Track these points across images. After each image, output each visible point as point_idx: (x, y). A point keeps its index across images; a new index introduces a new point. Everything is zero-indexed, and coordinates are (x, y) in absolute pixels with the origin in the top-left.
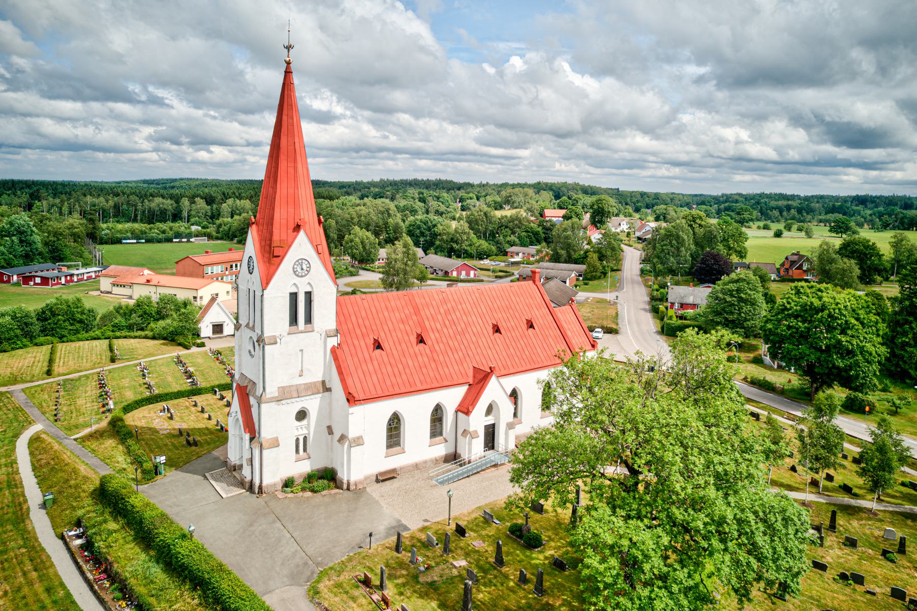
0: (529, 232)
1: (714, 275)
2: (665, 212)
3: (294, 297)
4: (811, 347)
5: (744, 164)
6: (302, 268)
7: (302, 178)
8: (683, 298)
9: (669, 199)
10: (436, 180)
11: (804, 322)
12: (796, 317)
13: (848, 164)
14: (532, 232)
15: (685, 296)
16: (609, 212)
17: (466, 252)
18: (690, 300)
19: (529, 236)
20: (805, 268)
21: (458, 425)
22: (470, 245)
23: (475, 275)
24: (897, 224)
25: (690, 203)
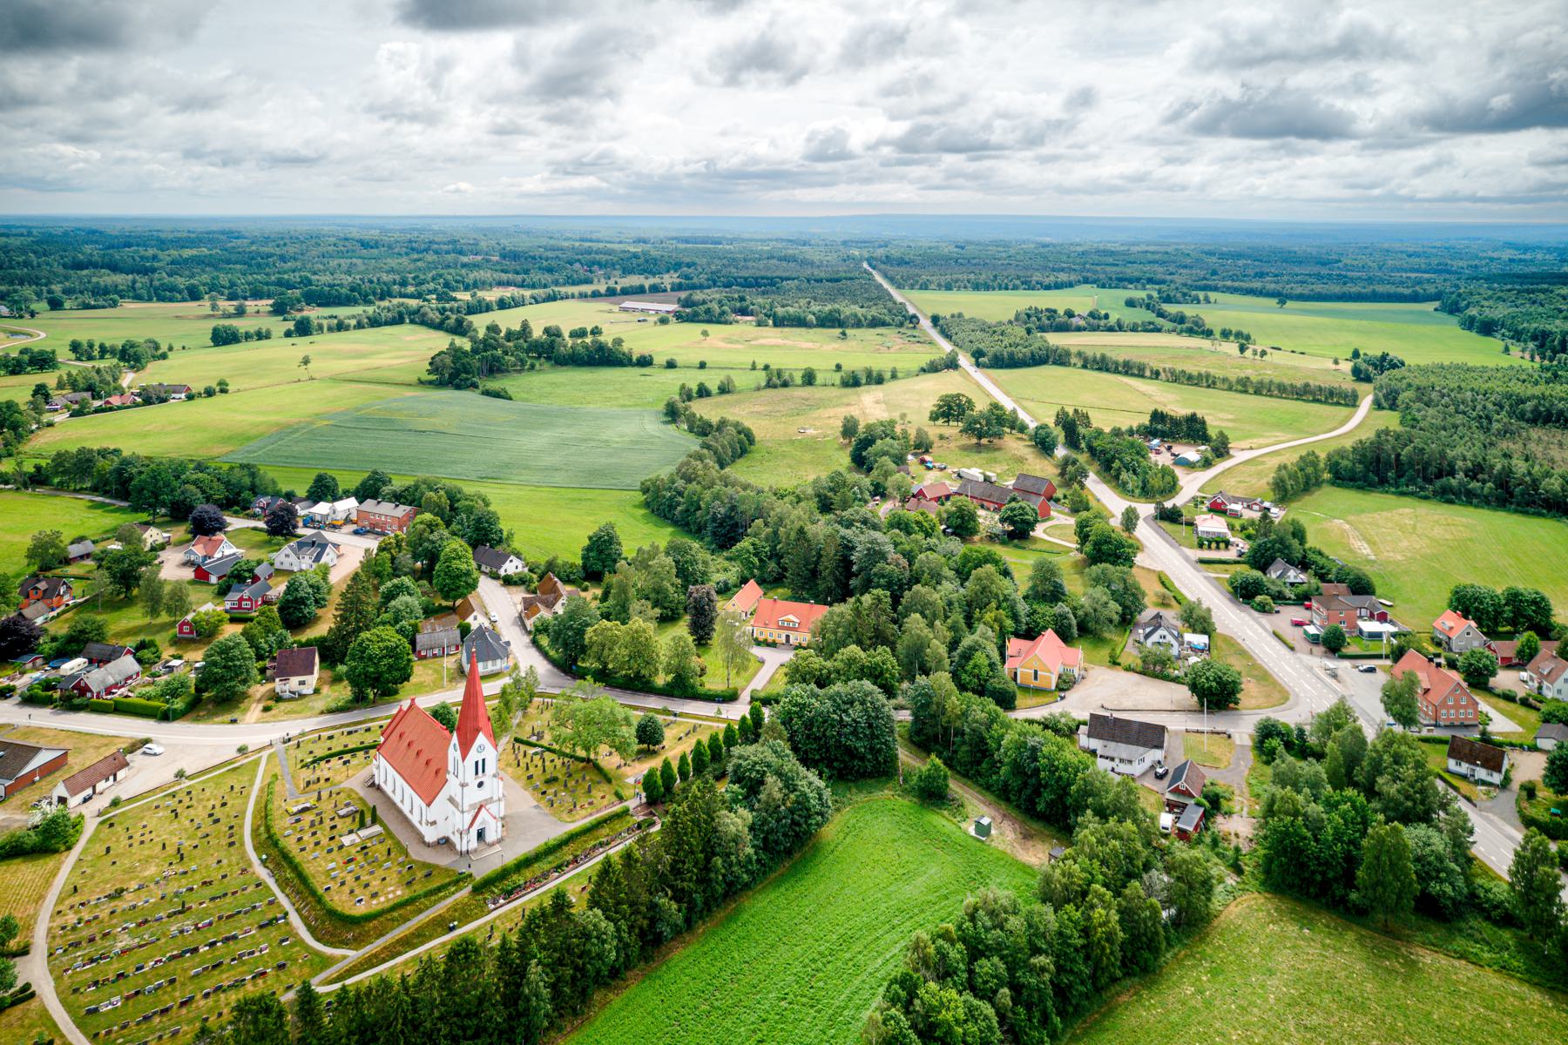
6: (481, 748)
18: (111, 681)
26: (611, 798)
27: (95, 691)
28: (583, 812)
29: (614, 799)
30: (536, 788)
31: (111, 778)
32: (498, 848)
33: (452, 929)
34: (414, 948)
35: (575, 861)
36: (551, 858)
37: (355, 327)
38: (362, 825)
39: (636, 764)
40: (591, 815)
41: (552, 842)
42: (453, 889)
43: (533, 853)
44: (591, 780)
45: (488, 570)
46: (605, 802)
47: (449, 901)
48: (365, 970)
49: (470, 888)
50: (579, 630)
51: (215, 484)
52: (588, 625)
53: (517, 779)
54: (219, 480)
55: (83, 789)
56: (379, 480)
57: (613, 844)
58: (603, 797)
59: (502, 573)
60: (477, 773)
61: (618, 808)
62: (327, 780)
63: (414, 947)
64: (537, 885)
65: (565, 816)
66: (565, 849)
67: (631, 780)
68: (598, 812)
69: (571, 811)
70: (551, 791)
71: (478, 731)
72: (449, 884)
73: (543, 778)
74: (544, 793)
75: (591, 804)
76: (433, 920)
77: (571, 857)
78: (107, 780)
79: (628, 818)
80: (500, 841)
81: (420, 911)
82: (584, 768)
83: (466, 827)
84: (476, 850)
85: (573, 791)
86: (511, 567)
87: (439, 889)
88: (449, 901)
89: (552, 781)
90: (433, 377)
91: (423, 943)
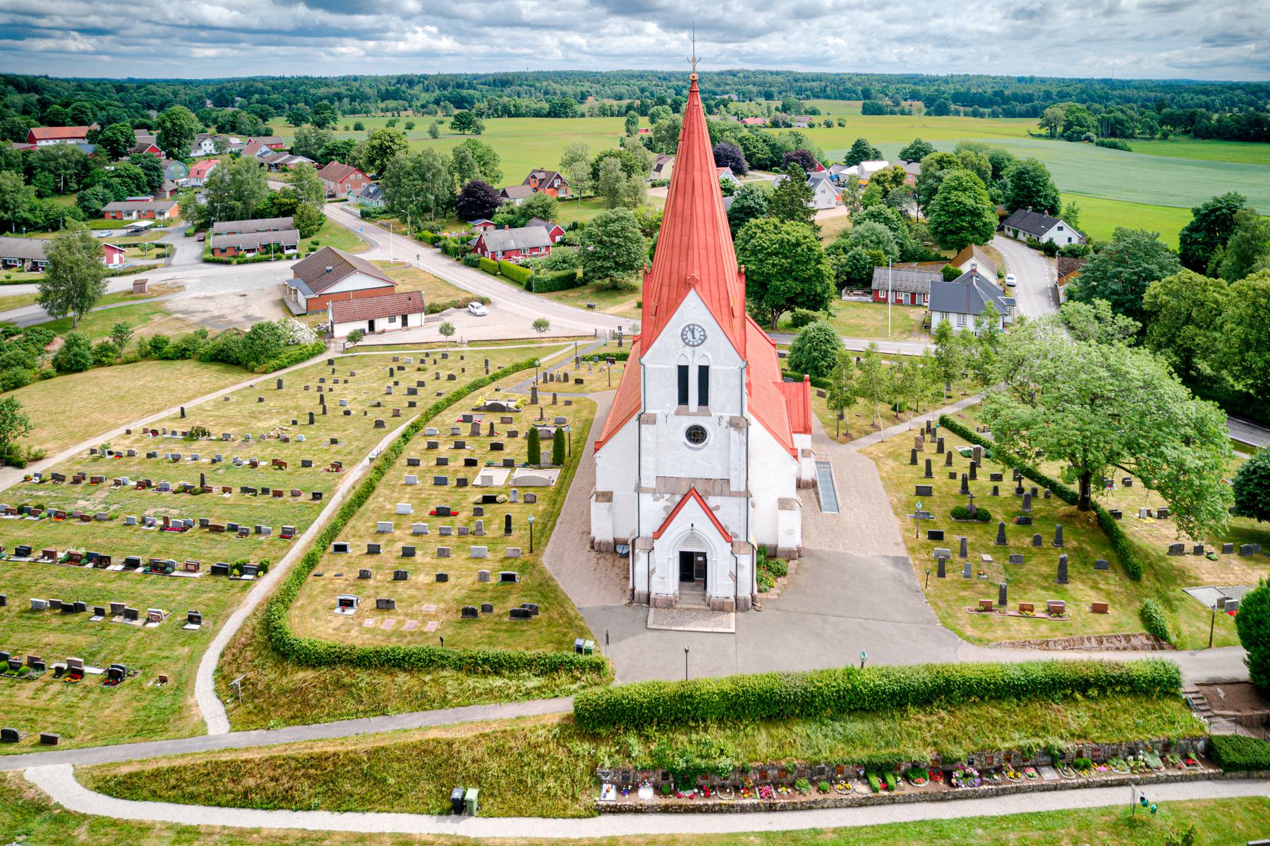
0: (123, 176)
1: (487, 208)
2: (231, 119)
3: (683, 372)
4: (796, 279)
5: (203, 34)
6: (693, 336)
7: (701, 225)
8: (503, 244)
9: (170, 95)
10: (1120, 235)
11: (786, 257)
12: (776, 254)
13: (341, 33)
14: (128, 176)
15: (505, 241)
16: (191, 130)
17: (25, 222)
18: (512, 245)
19: (125, 182)
20: (556, 186)
21: (642, 463)
22: (31, 210)
23: (121, 260)
24: (490, 112)
25: (202, 97)
26: (1123, 619)
27: (490, 248)
28: (1023, 628)
29: (1135, 626)
30: (923, 517)
31: (399, 320)
32: (729, 622)
33: (460, 808)
34: (338, 808)
35: (944, 769)
36: (857, 727)
37: (989, 115)
38: (534, 460)
39: (1234, 561)
40: (1045, 644)
41: (870, 677)
42: (534, 682)
43: (796, 686)
44: (1078, 551)
45: (1024, 239)
46: (1102, 625)
47: (500, 715)
48: (192, 799)
49: (563, 706)
50: (1135, 284)
51: (760, 145)
52: (1151, 277)
53: (891, 484)
54: (764, 141)
55: (353, 320)
56: (921, 150)
57: (1095, 774)
58: (1099, 609)
59: (1044, 239)
60: (683, 399)
61: (1139, 660)
62: (579, 381)
63: (339, 804)
64: (782, 795)
65: (964, 614)
66: (916, 717)
67: (1207, 597)
68: (1070, 645)
69: (988, 608)
70: (953, 538)
71: (688, 284)
72: (529, 664)
73: (953, 504)
74: (936, 536)
75: (1055, 611)
76: (424, 750)
77: (928, 755)
78: (392, 320)
79: (1171, 707)
80: (739, 606)
81: (422, 702)
82: (1069, 518)
83: (647, 530)
84: (669, 604)
85: (1017, 560)
86: (1060, 236)
87: (497, 666)
88: (500, 715)
89: (971, 516)
90: (1044, 131)
91: (365, 804)
